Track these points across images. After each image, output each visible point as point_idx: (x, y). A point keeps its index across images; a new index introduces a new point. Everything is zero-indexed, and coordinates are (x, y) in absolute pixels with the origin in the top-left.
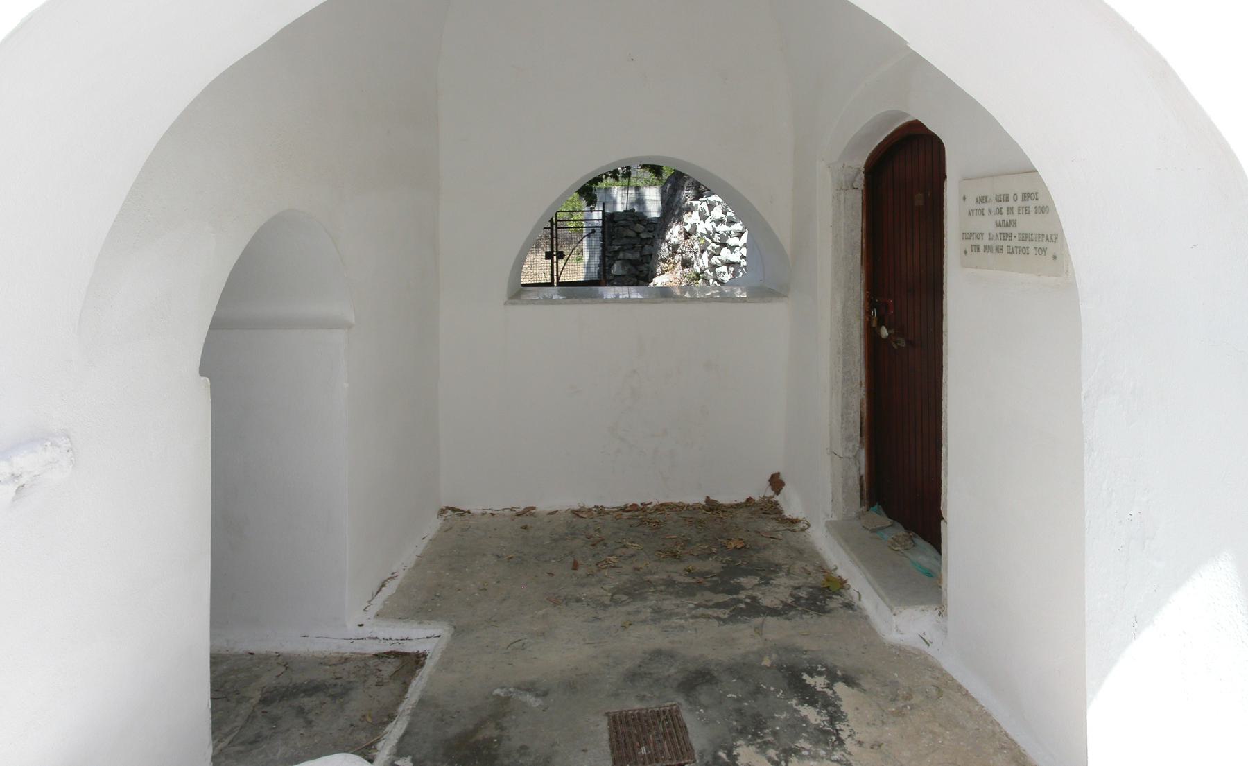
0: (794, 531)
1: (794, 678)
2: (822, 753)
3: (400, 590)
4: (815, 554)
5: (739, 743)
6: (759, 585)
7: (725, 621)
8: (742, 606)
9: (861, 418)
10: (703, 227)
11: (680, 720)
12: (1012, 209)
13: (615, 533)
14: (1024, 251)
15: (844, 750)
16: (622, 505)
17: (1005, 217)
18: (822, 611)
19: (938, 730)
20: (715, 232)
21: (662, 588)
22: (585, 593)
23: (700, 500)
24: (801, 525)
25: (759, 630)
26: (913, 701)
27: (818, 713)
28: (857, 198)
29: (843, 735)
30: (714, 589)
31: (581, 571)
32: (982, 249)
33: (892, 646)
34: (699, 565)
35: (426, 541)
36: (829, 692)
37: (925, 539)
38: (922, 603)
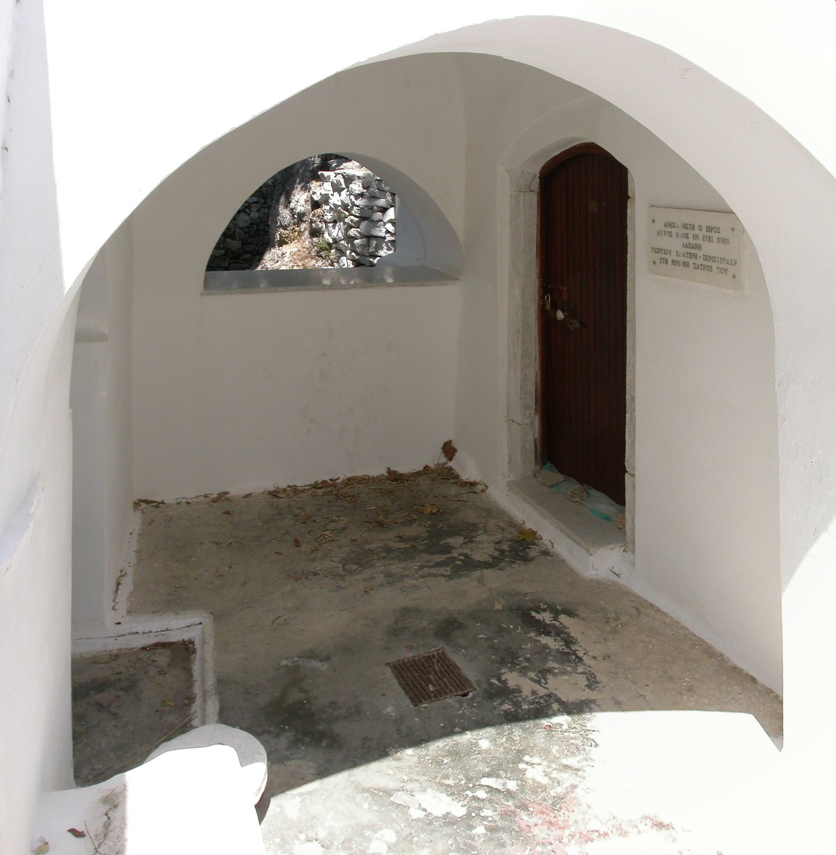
0: (475, 493)
1: (525, 615)
2: (569, 669)
3: (137, 586)
4: (501, 513)
5: (503, 671)
7: (450, 577)
8: (459, 563)
9: (536, 388)
10: (335, 199)
12: (697, 236)
13: (318, 510)
14: (709, 269)
15: (585, 664)
16: (312, 482)
17: (691, 241)
18: (526, 560)
19: (646, 639)
20: (354, 205)
21: (384, 554)
22: (318, 567)
23: (383, 471)
24: (480, 487)
25: (480, 580)
26: (621, 621)
27: (555, 640)
28: (533, 199)
29: (580, 654)
30: (429, 550)
31: (304, 548)
32: (670, 262)
33: (591, 581)
35: (135, 535)
36: (557, 624)
38: (610, 543)
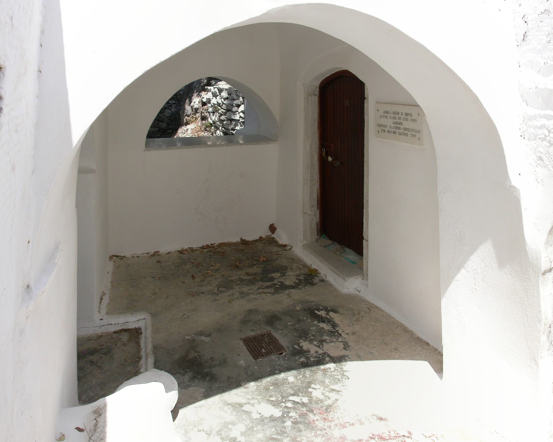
0: (286, 250)
1: (312, 312)
2: (335, 340)
4: (299, 261)
5: (301, 341)
6: (281, 276)
10: (214, 101)
11: (273, 336)
13: (204, 260)
14: (406, 135)
16: (201, 246)
17: (397, 120)
18: (313, 284)
20: (223, 103)
21: (239, 282)
22: (204, 289)
24: (289, 247)
25: (289, 295)
28: (316, 99)
29: (340, 332)
30: (262, 280)
31: (197, 279)
33: (346, 295)
34: (250, 271)
35: (110, 273)
36: (328, 317)
37: (349, 247)
38: (356, 275)
